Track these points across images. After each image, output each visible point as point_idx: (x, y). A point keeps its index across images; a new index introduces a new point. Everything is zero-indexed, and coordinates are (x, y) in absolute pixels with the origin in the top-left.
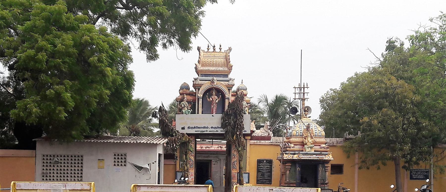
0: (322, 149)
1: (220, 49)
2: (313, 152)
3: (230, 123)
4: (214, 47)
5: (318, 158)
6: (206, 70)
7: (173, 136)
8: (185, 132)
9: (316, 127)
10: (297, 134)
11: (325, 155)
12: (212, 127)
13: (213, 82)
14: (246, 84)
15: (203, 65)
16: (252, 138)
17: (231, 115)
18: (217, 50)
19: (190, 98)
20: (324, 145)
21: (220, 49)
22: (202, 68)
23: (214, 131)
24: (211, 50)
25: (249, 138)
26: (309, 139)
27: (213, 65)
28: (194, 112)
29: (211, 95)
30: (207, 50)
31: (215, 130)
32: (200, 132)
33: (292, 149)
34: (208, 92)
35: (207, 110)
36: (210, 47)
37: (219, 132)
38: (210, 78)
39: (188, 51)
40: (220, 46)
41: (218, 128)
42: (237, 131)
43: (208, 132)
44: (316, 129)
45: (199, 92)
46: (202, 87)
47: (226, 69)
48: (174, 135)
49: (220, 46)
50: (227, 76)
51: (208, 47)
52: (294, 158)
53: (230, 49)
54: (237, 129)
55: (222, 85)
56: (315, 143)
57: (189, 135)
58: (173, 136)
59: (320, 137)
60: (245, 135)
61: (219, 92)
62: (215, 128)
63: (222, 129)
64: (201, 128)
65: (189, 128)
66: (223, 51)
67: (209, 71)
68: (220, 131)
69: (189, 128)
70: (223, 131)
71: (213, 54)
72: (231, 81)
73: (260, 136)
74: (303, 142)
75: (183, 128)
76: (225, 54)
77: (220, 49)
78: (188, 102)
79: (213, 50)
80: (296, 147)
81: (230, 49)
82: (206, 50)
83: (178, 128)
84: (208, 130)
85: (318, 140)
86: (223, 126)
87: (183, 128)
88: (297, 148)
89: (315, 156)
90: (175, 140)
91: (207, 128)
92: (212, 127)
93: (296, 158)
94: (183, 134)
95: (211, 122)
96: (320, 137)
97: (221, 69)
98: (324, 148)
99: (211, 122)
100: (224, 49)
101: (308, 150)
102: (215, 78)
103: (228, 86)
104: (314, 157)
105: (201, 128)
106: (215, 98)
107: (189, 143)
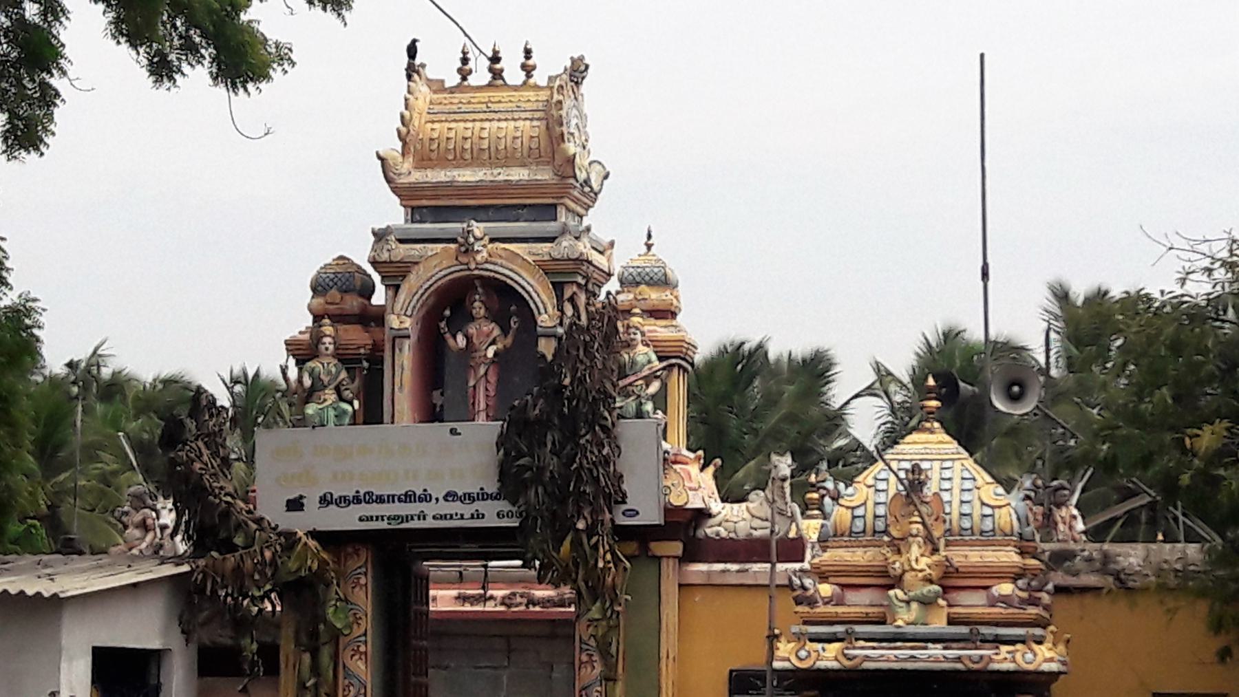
0: (999, 611)
1: (524, 67)
2: (938, 624)
3: (541, 470)
4: (495, 59)
5: (959, 659)
6: (437, 186)
7: (233, 548)
8: (299, 524)
9: (968, 485)
10: (859, 524)
11: (998, 641)
12: (450, 496)
13: (468, 250)
14: (672, 256)
15: (424, 160)
16: (697, 550)
17: (543, 424)
18: (514, 75)
19: (356, 336)
20: (1006, 588)
21: (528, 70)
22: (417, 176)
23: (462, 516)
24: (481, 76)
25: (677, 548)
26: (915, 551)
27: (477, 157)
28: (372, 413)
29: (461, 317)
30: (457, 79)
31: (467, 509)
32: (383, 525)
33: (821, 609)
34: (451, 303)
35: (439, 400)
36: (471, 65)
37: (491, 521)
38: (454, 227)
39: (250, 86)
40: (528, 53)
41: (484, 496)
42: (580, 514)
43: (429, 523)
44: (967, 497)
45: (398, 307)
46: (412, 277)
47: (545, 175)
48: (239, 540)
49: (528, 53)
50: (549, 211)
51: (465, 60)
52: (822, 664)
53: (577, 72)
54: (576, 503)
55: (516, 260)
56: (950, 580)
57: (330, 540)
58: (233, 548)
59: (988, 538)
60: (645, 535)
61: (506, 300)
62: (469, 498)
63: (504, 506)
64: (391, 498)
65: (325, 501)
66: (539, 78)
67: (451, 188)
68: (494, 515)
69: (325, 501)
70: (509, 515)
71: (496, 95)
72: (566, 242)
73: (742, 535)
74: (884, 573)
75: (295, 505)
76: (543, 95)
77: (528, 70)
78: (345, 358)
79: (486, 78)
80: (851, 596)
81: (577, 72)
82: (453, 80)
83: (270, 507)
84: (430, 509)
85: (974, 556)
86: (511, 482)
87: (295, 505)
88: (860, 602)
89: (936, 651)
90: (238, 569)
91: (426, 498)
92: (450, 496)
93: (834, 665)
94: (290, 539)
95: (440, 465)
96: (988, 538)
97: (518, 174)
98: (1005, 600)
99: (440, 465)
100: (549, 66)
101: (905, 618)
102: (478, 228)
103: (552, 266)
104: (934, 656)
105: (391, 498)
106: (485, 337)
107: (328, 585)
